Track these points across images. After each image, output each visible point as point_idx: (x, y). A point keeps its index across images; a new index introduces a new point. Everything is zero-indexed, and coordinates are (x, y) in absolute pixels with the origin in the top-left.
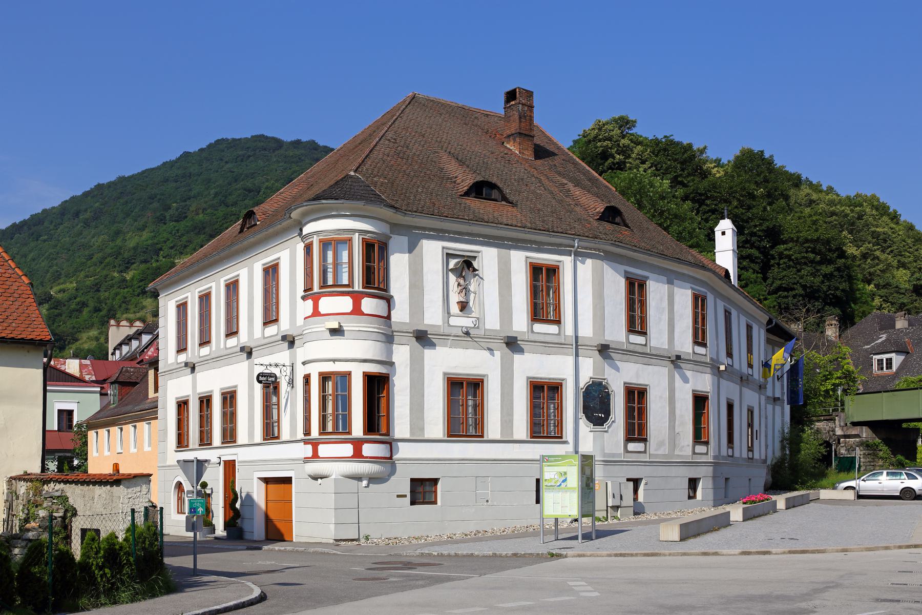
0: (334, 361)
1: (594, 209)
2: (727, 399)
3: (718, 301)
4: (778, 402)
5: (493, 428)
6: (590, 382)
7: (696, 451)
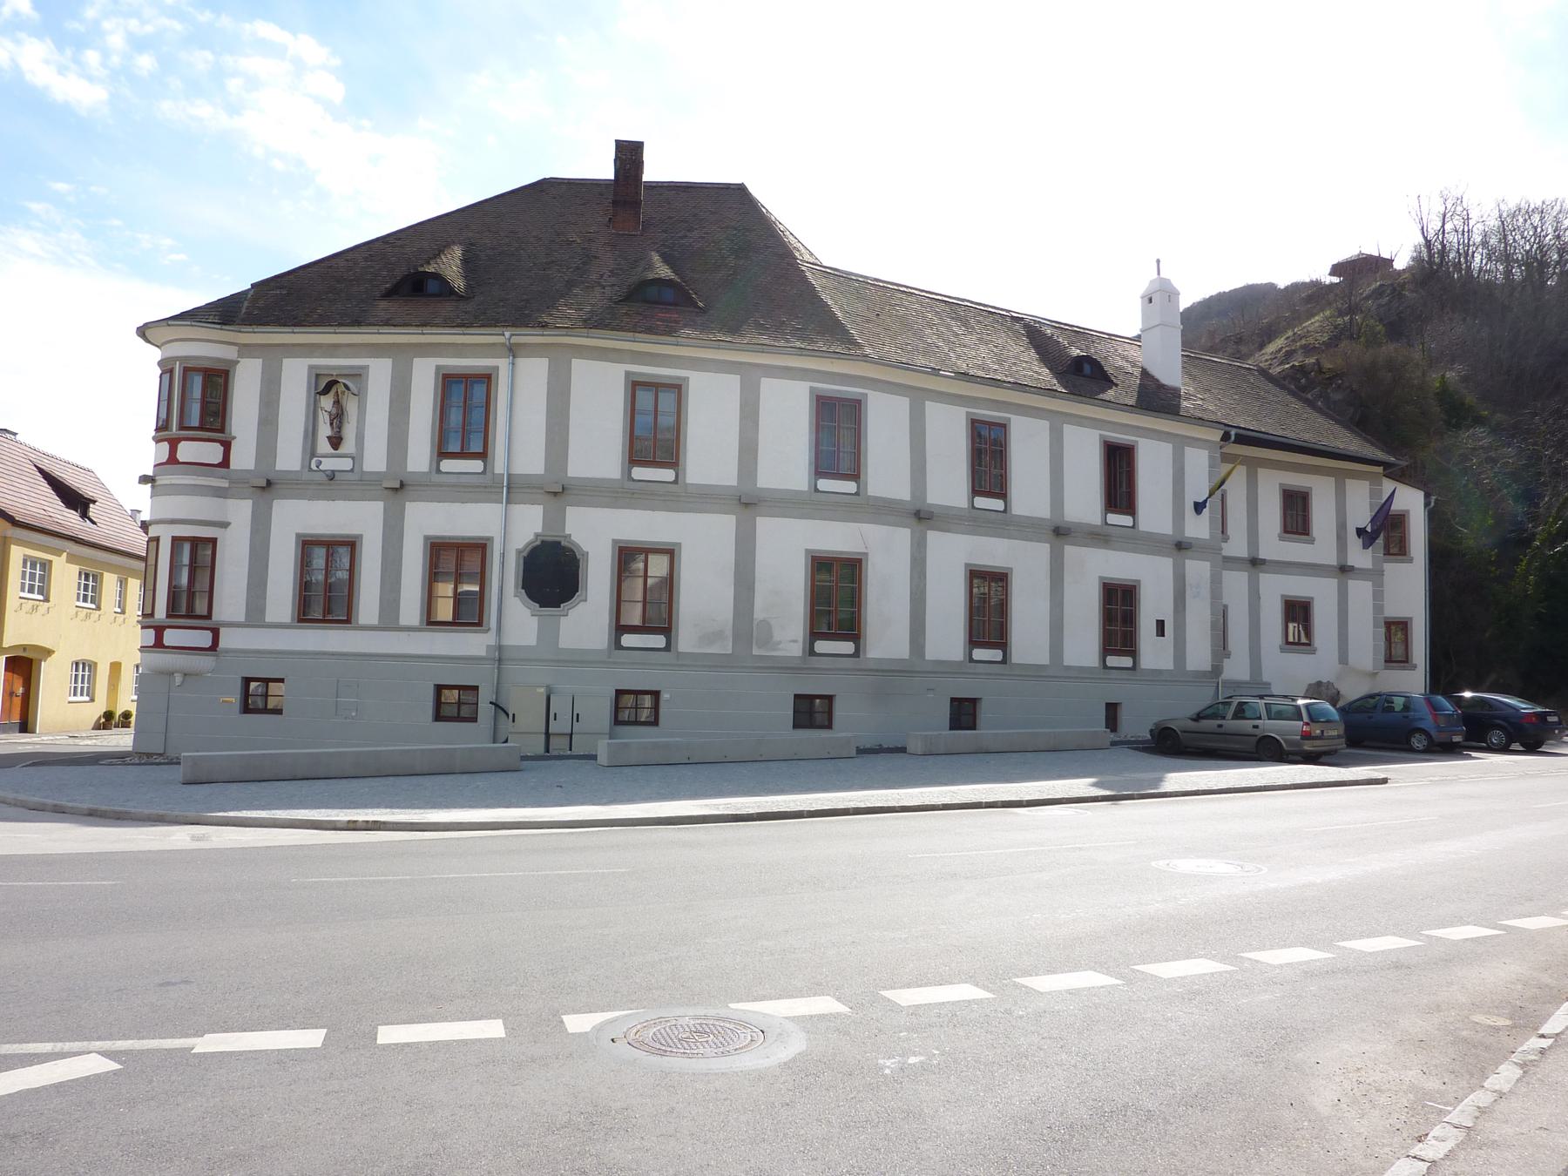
6: (537, 540)
7: (975, 657)
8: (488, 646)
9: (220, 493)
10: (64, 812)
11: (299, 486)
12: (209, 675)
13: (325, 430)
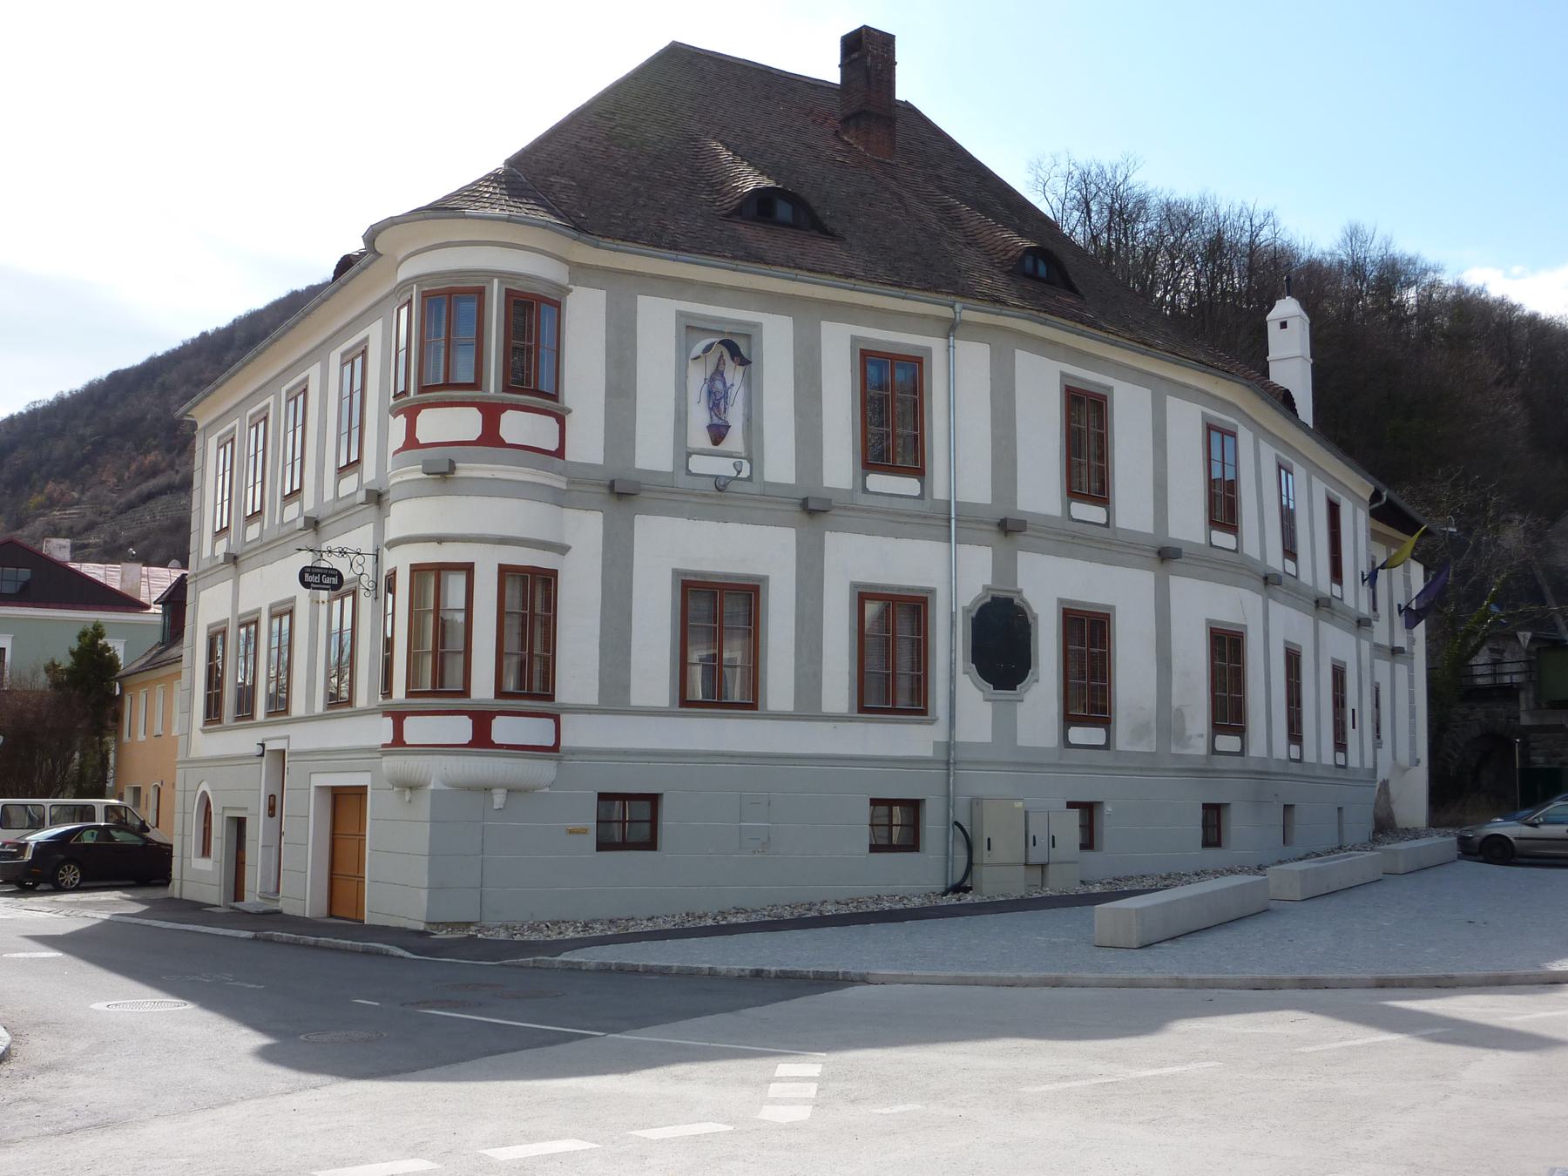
0: (440, 540)
1: (1004, 253)
2: (1286, 642)
3: (1264, 446)
4: (1399, 657)
5: (779, 687)
8: (935, 743)
9: (559, 499)
10: (1326, 988)
11: (673, 497)
12: (547, 790)
13: (699, 416)
